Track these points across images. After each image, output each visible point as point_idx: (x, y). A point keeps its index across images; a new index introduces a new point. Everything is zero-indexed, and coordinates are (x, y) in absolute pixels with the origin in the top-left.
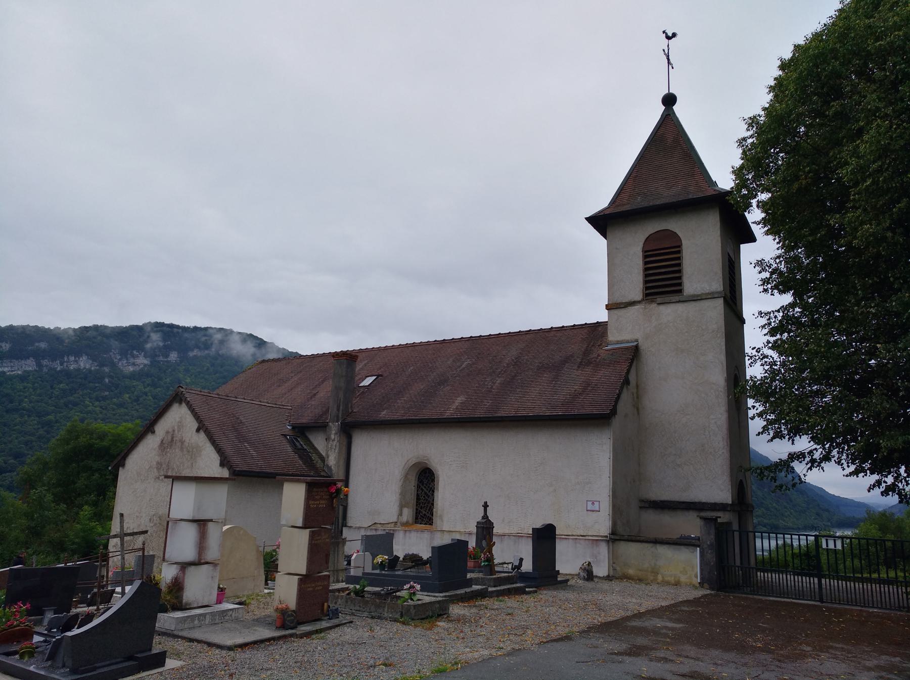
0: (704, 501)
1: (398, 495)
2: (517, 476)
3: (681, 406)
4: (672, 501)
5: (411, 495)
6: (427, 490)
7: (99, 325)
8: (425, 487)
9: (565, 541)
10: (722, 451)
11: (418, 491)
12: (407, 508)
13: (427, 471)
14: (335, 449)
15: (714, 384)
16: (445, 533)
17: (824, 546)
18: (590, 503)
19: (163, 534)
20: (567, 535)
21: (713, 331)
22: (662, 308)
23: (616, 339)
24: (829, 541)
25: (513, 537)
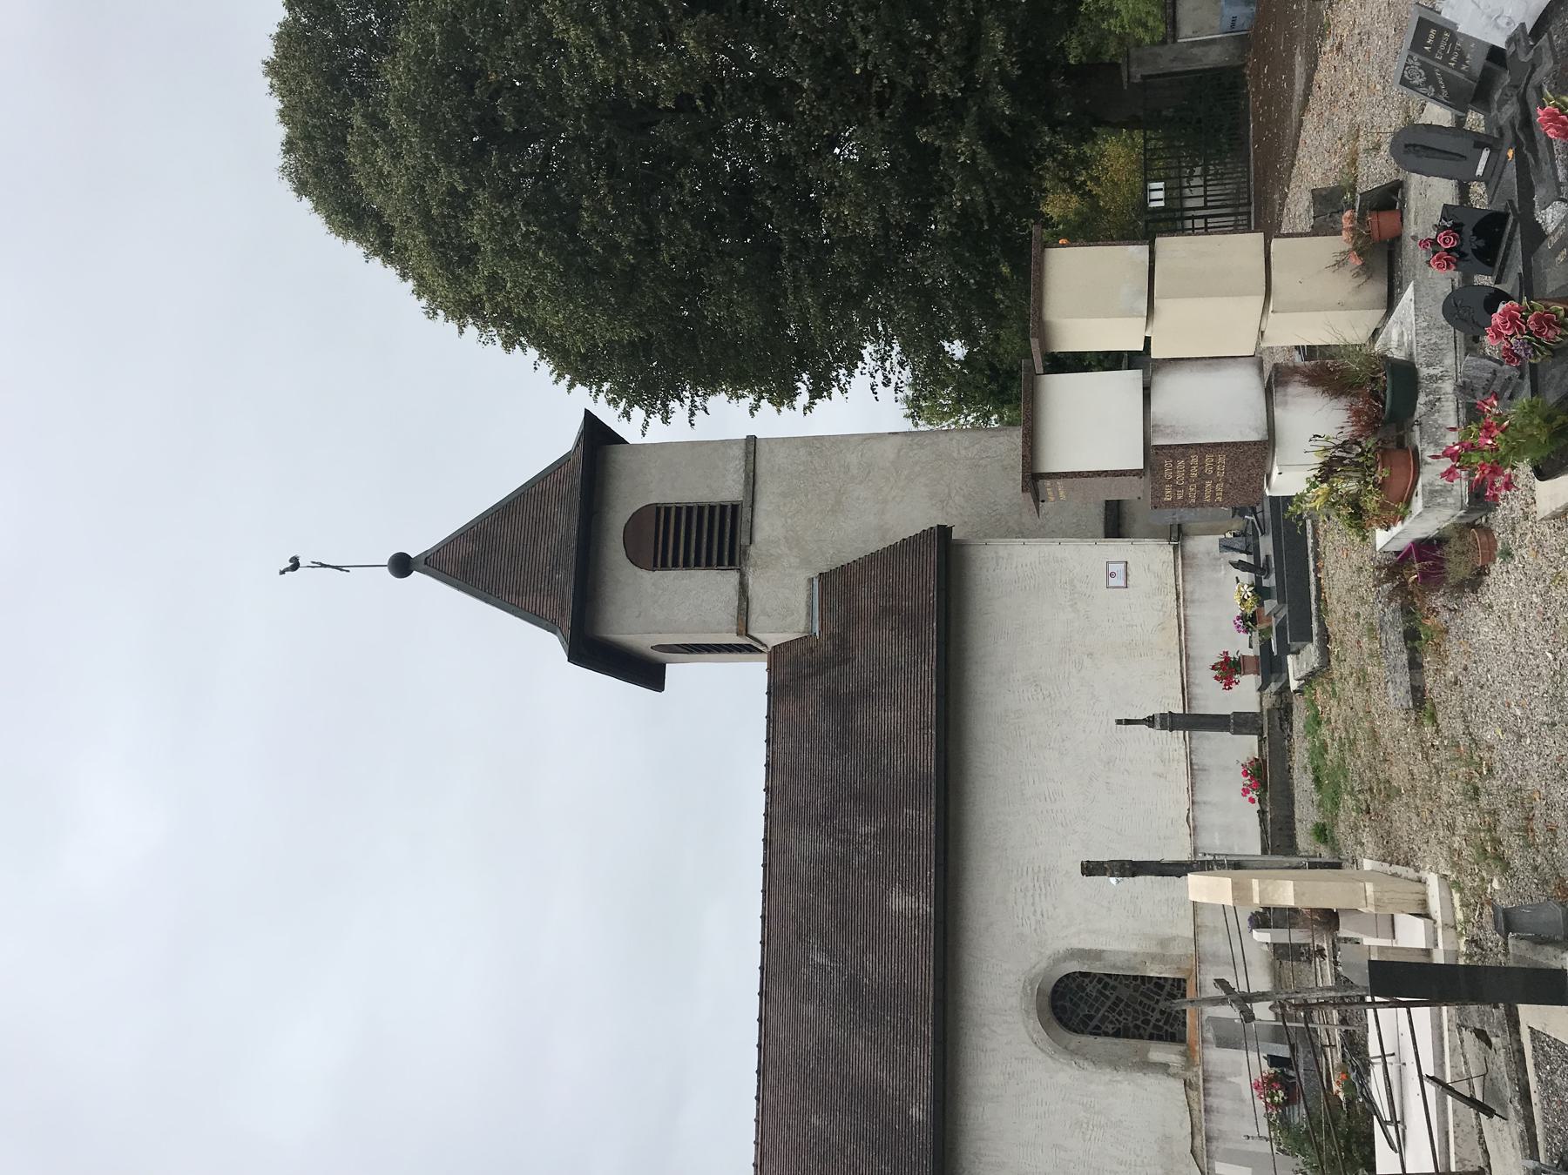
1: (1120, 1076)
2: (1063, 740)
4: (1106, 518)
5: (1116, 1044)
6: (1103, 1004)
8: (1098, 1010)
9: (1191, 625)
10: (1015, 438)
11: (1106, 1034)
15: (899, 451)
16: (1198, 798)
17: (1162, 204)
18: (1113, 582)
20: (1180, 630)
21: (810, 454)
22: (758, 537)
23: (804, 618)
24: (1153, 198)
25: (1194, 742)
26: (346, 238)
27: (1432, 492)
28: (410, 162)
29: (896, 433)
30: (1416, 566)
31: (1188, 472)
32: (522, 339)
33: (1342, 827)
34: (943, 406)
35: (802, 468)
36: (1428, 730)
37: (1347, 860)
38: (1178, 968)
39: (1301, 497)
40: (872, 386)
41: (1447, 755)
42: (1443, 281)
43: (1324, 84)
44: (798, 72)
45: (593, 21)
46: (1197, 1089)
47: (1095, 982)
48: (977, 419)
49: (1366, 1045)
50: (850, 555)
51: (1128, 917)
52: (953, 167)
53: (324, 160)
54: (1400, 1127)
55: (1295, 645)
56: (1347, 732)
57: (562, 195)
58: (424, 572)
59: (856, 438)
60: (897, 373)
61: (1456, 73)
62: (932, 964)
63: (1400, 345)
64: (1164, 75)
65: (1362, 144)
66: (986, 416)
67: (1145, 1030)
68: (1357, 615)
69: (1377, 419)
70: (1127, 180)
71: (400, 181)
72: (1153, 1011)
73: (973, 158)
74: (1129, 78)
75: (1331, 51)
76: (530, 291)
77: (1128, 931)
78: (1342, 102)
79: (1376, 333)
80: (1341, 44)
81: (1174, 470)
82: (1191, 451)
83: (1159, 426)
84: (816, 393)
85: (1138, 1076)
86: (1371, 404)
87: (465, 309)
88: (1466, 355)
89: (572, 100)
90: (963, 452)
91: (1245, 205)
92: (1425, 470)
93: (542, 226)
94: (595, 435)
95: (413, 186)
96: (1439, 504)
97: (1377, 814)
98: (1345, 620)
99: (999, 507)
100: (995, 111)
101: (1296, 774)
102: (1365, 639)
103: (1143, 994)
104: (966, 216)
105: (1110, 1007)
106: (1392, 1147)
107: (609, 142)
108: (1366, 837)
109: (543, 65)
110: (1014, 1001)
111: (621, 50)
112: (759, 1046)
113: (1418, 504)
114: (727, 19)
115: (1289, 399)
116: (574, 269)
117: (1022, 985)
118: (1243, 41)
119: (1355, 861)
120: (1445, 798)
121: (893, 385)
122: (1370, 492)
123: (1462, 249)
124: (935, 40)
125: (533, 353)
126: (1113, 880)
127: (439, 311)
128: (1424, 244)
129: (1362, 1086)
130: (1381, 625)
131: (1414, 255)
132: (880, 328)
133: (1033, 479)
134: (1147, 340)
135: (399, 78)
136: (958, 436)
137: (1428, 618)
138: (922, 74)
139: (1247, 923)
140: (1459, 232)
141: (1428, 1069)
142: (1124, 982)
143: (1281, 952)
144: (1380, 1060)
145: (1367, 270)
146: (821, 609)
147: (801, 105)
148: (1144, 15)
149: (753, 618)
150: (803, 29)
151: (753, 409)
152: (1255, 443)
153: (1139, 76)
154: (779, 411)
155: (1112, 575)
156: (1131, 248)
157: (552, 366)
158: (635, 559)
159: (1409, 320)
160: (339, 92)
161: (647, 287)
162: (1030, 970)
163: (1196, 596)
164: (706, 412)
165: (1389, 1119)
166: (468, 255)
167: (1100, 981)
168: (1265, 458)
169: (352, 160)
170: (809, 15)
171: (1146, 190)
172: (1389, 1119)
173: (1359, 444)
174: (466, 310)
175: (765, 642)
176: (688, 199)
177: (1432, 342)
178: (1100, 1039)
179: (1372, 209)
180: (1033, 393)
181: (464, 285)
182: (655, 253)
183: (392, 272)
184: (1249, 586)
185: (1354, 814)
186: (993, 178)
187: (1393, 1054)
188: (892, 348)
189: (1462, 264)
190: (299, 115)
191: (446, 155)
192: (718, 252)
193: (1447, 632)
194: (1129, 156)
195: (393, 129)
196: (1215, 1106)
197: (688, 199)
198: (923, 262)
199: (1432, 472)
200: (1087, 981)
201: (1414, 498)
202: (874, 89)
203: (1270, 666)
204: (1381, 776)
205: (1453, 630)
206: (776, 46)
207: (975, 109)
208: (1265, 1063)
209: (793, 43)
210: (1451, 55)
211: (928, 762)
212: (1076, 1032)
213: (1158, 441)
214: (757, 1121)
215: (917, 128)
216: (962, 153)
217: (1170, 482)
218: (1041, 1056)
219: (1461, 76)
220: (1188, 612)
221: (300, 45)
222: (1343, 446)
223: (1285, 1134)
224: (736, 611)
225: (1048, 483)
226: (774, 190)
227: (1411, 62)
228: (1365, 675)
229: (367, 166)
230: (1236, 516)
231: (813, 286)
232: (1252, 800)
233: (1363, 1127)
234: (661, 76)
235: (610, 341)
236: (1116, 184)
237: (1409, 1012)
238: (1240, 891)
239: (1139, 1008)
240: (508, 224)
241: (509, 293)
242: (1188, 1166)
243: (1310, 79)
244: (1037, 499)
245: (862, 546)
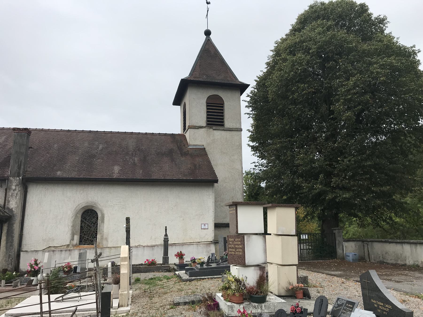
1: (70, 228)
2: (160, 212)
3: (223, 179)
4: (219, 223)
6: (89, 223)
8: (88, 222)
9: (191, 246)
11: (81, 224)
12: (76, 235)
13: (89, 211)
14: (16, 197)
15: (237, 169)
17: (302, 238)
18: (203, 225)
20: (190, 243)
21: (237, 146)
22: (215, 131)
25: (160, 247)
26: (297, 19)
27: (232, 307)
28: (318, 37)
29: (242, 169)
30: (212, 303)
31: (237, 245)
32: (269, 67)
33: (140, 285)
34: (248, 180)
35: (233, 143)
36: (168, 307)
37: (131, 287)
38: (99, 243)
39: (230, 274)
40: (255, 162)
41: (162, 311)
42: (288, 309)
43: (334, 279)
44: (339, 143)
45: (354, 88)
46: (67, 248)
47: (95, 221)
48: (245, 190)
49: (84, 292)
50: (210, 156)
51: (113, 230)
52: (313, 184)
53: (319, 13)
54: (62, 301)
55: (188, 273)
56: (166, 286)
57: (308, 79)
58: (206, 39)
59: (241, 157)
60: (258, 169)
61: (341, 312)
62: (100, 177)
63: (270, 299)
64: (335, 239)
65: (319, 289)
66: (245, 192)
67: (83, 234)
68: (197, 289)
69: (251, 293)
70: (307, 229)
71: (312, 34)
72: (88, 236)
73: (316, 189)
74: (334, 229)
75: (342, 281)
76: (282, 70)
78: (329, 284)
79: (272, 293)
80: (344, 283)
81: (238, 241)
82: (243, 245)
83: (249, 237)
84: (253, 147)
85: (70, 232)
86: (255, 292)
87: (278, 52)
88: (270, 315)
89: (333, 82)
90: (237, 186)
91: (301, 259)
92: (238, 305)
93: (300, 73)
94: (243, 87)
95: (311, 38)
96: (229, 309)
97: (144, 294)
98: (196, 286)
99: (222, 195)
100: (327, 195)
101: (152, 273)
102: (191, 291)
103: (92, 233)
104: (300, 187)
105: (88, 225)
106: (56, 299)
107: (322, 92)
108: (138, 292)
109: (343, 74)
110: (90, 199)
111: (346, 96)
112: (76, 130)
113: (229, 304)
114: (353, 124)
115: (256, 271)
116: (288, 82)
117: (94, 201)
118: (343, 259)
119: (131, 289)
120: (151, 311)
121: (255, 168)
122: (232, 292)
123: (296, 314)
124: (346, 179)
125: (265, 70)
126: (125, 226)
127: (277, 45)
128: (298, 304)
129: (72, 291)
130: (195, 295)
131: (295, 302)
132: (270, 164)
133: (235, 205)
134: (270, 234)
135: (341, 35)
136: (241, 185)
137: (198, 307)
138: (338, 175)
139: (112, 261)
140: (300, 313)
141: (79, 308)
143: (105, 270)
144: (79, 295)
145: (288, 290)
146: (195, 148)
147: (330, 144)
148: (349, 233)
150: (350, 144)
151: (249, 131)
152: (245, 262)
153: (335, 232)
154: (248, 137)
155: (205, 225)
156: (295, 230)
157: (261, 76)
158: (209, 98)
159: (276, 301)
160: (337, 18)
161: (283, 102)
163: (199, 247)
164: (249, 118)
165: (63, 298)
166: (292, 53)
167: (96, 222)
168: (241, 265)
169: (319, 21)
170: (354, 146)
171: (305, 234)
172: (63, 298)
173: (245, 289)
174: (277, 52)
175: (186, 133)
176: (306, 113)
177: (271, 307)
178: (80, 222)
179: (304, 291)
180: (259, 204)
181: (284, 52)
182: (291, 104)
183: (288, 32)
184: (204, 261)
185: (144, 288)
186: (309, 194)
187: (81, 299)
188: (265, 168)
189: (292, 314)
190: (331, 6)
192: (292, 121)
193: (194, 311)
194: (313, 229)
195: (327, 33)
196: (62, 253)
197: (306, 113)
198: (288, 176)
199: (237, 307)
200: (96, 219)
201: (230, 303)
202: (334, 163)
203: (181, 266)
204: (155, 295)
205: (195, 313)
206: (346, 137)
207: (328, 189)
208: (75, 266)
209: (347, 142)
210: (346, 311)
211: (155, 177)
212: (82, 216)
213: (246, 237)
214: (55, 130)
215: (323, 174)
216: (316, 186)
217: (234, 240)
218: (75, 207)
219: (340, 313)
220: (195, 245)
221: (350, 7)
222: (244, 285)
223: (57, 271)
224: (195, 125)
225: (234, 208)
226: (308, 136)
227: (344, 300)
228: (182, 291)
229: (317, 25)
230: (220, 258)
231: (282, 146)
232: (145, 262)
233: (59, 291)
234: (338, 106)
235: (268, 92)
236: (306, 226)
237: (95, 302)
238: (124, 259)
239: (88, 233)
240: (301, 64)
241: (282, 64)
242: (46, 246)
243: (335, 275)
244: (230, 206)
245: (213, 159)
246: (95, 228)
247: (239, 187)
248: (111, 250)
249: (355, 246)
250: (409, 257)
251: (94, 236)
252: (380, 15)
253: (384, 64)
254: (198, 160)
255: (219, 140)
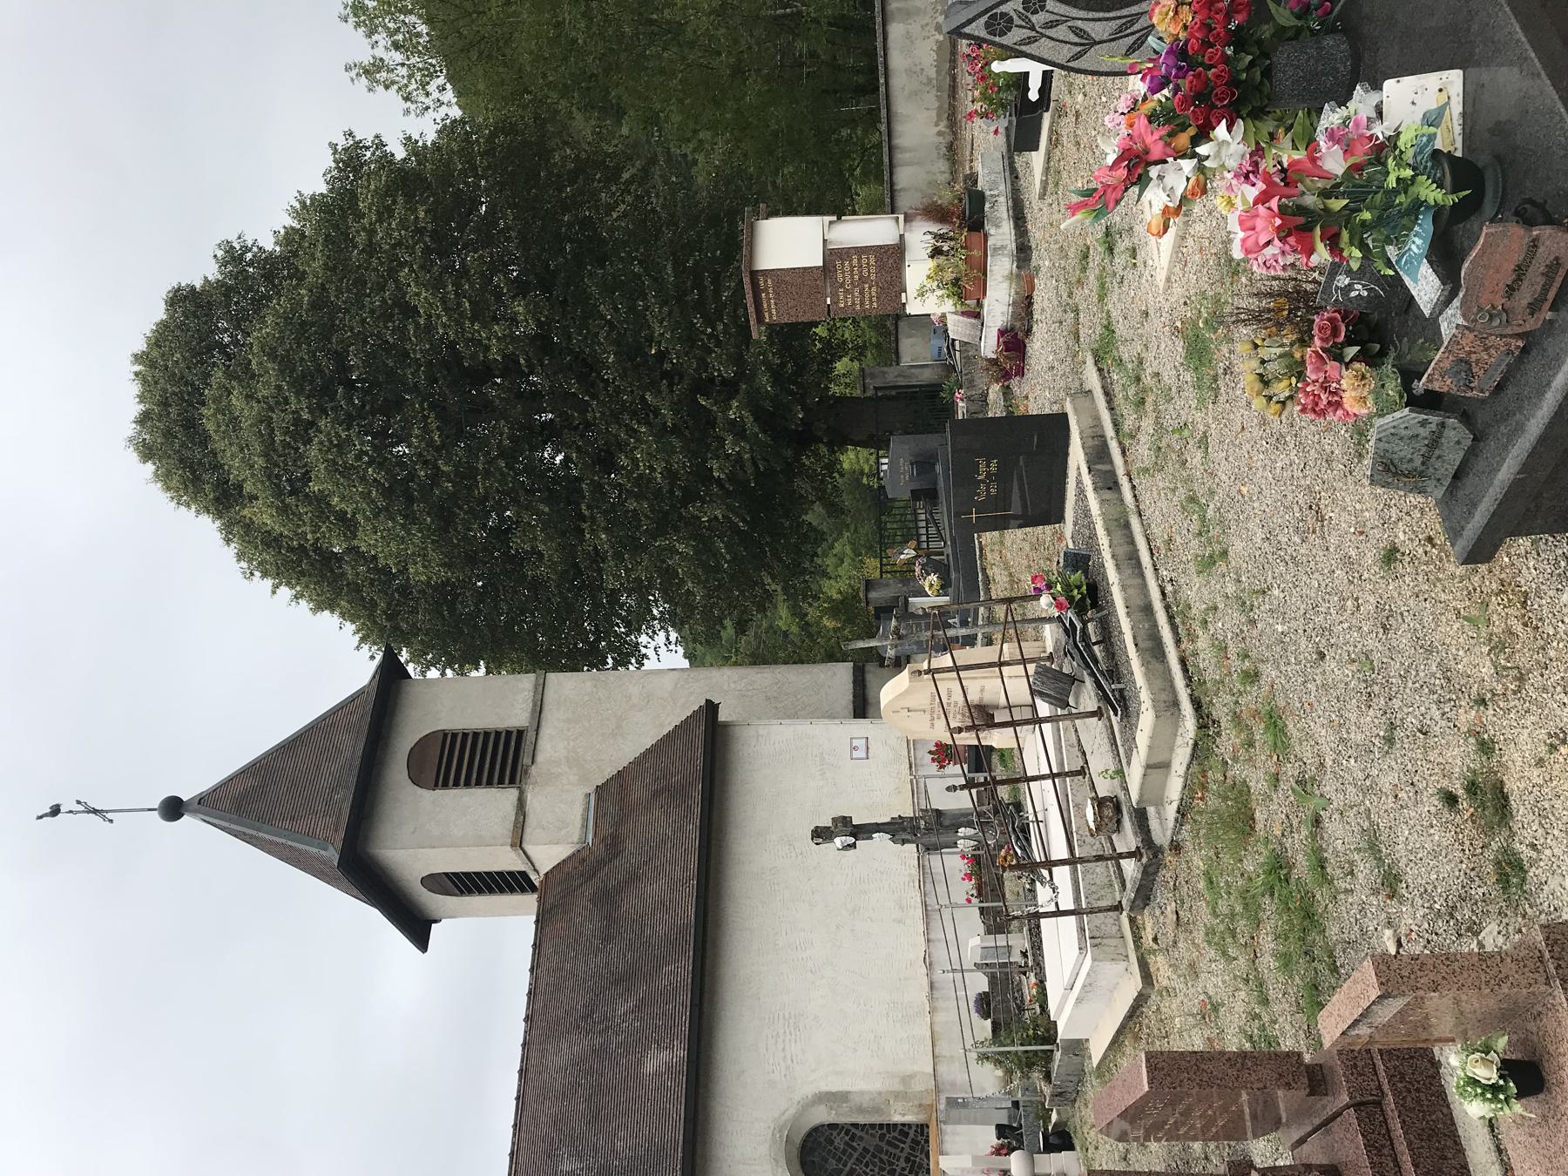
0: (851, 697)
2: (813, 893)
6: (851, 1156)
7: (318, 186)
8: (845, 1165)
18: (856, 755)
19: (936, 1028)
22: (540, 758)
35: (587, 698)
72: (898, 1160)
77: (872, 1069)
90: (732, 685)
103: (889, 1143)
105: (857, 1159)
110: (764, 1149)
111: (462, 314)
142: (870, 1132)
146: (596, 812)
149: (528, 830)
155: (855, 748)
158: (417, 780)
162: (780, 1117)
171: (878, 463)
191: (298, 386)
200: (835, 1133)
211: (687, 910)
239: (885, 1157)
246: (867, 1133)
247: (736, 678)
248: (945, 1057)
249: (911, 337)
250: (928, 173)
251: (896, 1134)
252: (215, 256)
253: (378, 211)
254: (638, 792)
255: (572, 744)
